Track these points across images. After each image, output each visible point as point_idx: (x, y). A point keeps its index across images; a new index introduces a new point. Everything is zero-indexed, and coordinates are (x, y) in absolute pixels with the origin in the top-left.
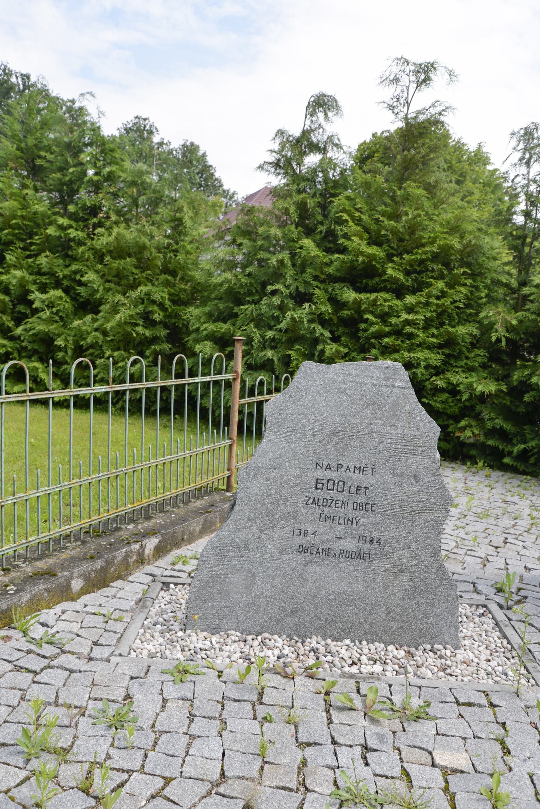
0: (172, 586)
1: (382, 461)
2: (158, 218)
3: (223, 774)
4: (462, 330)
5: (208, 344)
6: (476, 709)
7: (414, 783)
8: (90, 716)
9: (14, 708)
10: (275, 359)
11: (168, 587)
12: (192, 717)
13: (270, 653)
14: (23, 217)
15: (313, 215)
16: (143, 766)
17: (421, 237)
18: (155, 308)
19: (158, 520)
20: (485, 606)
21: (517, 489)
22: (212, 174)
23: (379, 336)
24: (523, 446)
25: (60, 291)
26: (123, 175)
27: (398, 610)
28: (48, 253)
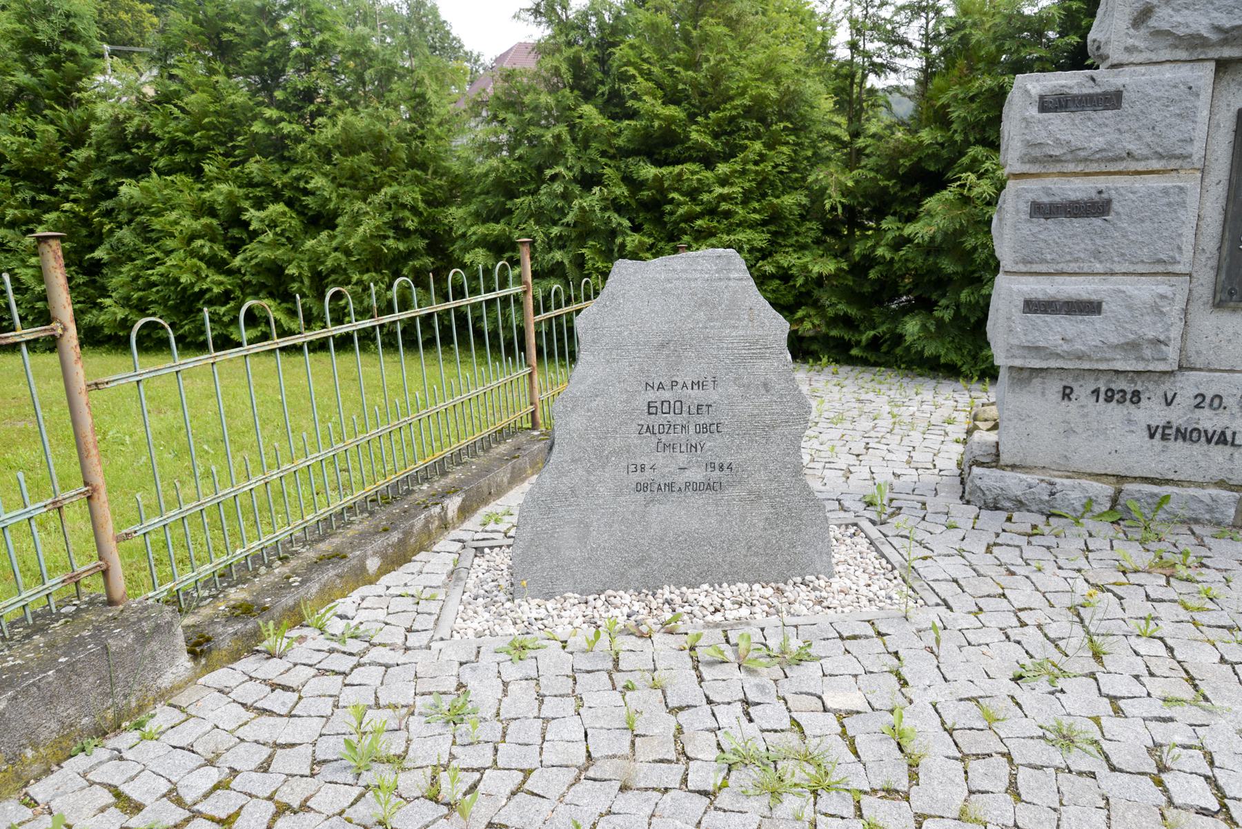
0: (487, 550)
1: (724, 371)
2: (393, 96)
3: (589, 756)
4: (788, 200)
5: (480, 251)
6: (863, 641)
7: (807, 733)
8: (421, 714)
9: (328, 718)
10: (566, 262)
11: (483, 552)
12: (541, 698)
13: (617, 612)
14: (217, 113)
15: (590, 73)
16: (495, 762)
17: (728, 88)
18: (407, 213)
19: (457, 475)
20: (856, 525)
21: (870, 385)
22: (448, 33)
23: (690, 218)
24: (872, 333)
25: (282, 204)
26: (340, 44)
27: (761, 543)
28: (258, 157)
